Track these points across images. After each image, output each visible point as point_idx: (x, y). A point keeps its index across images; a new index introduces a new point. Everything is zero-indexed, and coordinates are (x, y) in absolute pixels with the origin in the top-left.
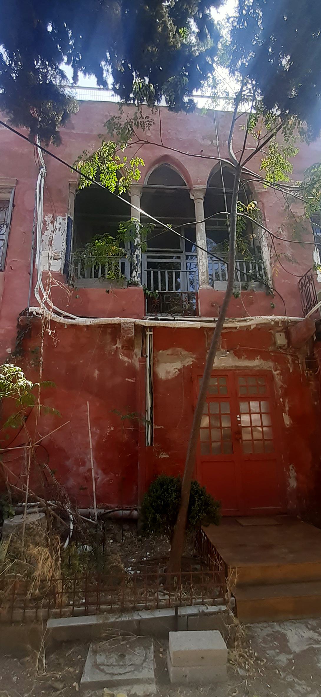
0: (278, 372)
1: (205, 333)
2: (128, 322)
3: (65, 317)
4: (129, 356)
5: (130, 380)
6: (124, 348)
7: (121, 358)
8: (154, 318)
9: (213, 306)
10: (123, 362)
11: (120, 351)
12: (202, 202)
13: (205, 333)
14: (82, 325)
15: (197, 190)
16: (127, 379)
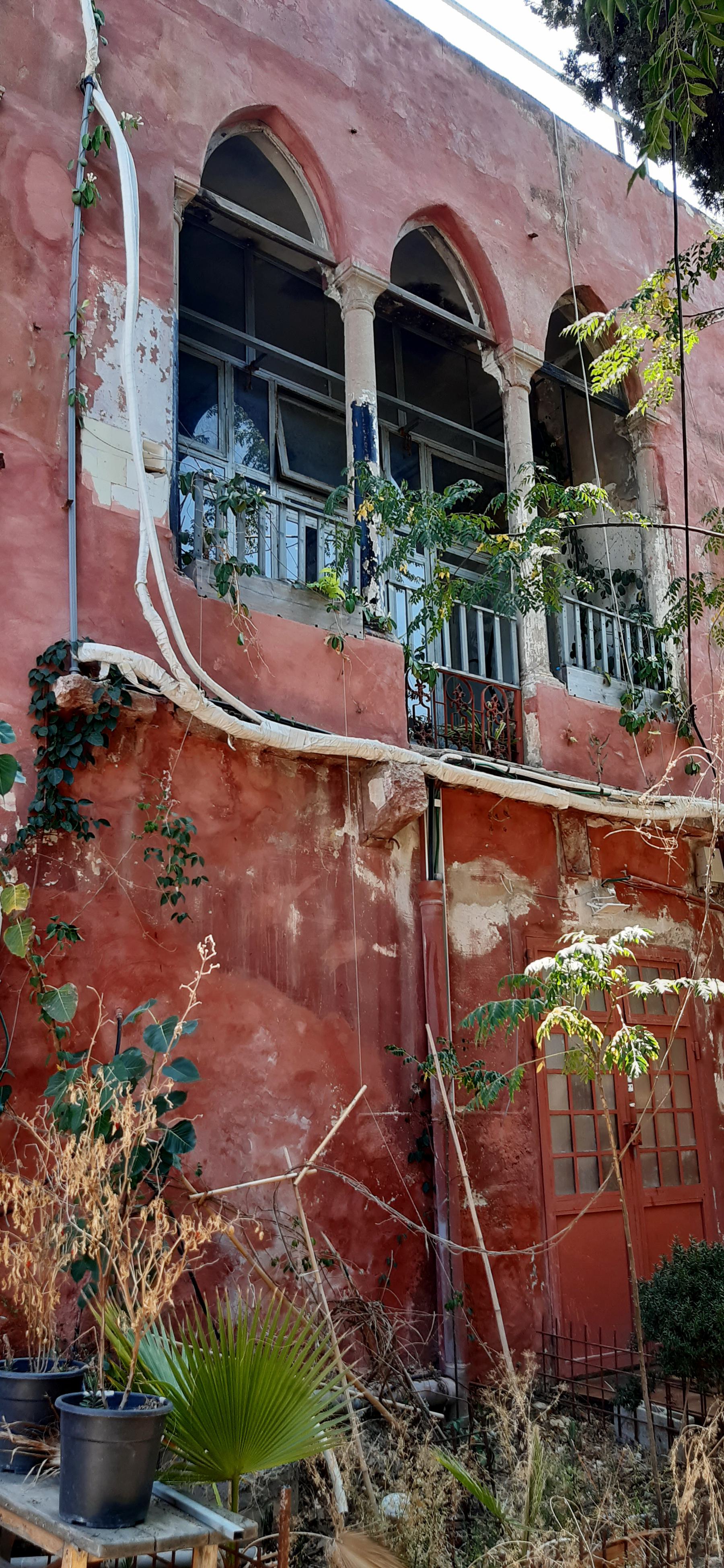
0: (702, 957)
1: (555, 822)
2: (404, 760)
3: (231, 710)
4: (380, 869)
5: (384, 951)
6: (370, 841)
7: (358, 873)
8: (460, 758)
9: (569, 742)
10: (363, 889)
11: (355, 847)
12: (526, 395)
13: (555, 822)
14: (278, 746)
15: (519, 358)
16: (376, 947)
